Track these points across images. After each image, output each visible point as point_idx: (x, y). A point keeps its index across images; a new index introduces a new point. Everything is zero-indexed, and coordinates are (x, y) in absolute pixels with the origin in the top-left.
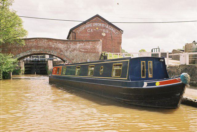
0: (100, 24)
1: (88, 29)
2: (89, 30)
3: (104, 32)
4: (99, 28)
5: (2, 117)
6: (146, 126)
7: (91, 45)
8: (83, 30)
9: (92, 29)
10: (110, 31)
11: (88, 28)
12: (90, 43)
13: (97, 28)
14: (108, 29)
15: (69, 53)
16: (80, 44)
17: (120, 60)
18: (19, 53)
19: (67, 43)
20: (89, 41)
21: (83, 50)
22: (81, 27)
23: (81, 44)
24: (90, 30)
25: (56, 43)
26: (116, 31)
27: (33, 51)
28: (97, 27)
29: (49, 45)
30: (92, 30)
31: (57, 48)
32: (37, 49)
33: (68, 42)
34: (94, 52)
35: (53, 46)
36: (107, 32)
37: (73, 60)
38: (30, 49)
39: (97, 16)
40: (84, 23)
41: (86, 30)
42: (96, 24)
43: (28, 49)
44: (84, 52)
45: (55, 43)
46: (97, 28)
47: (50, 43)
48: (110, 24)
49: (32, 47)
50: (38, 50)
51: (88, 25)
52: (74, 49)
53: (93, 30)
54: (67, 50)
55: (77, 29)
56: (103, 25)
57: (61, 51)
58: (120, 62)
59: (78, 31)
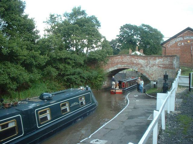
1: (179, 43)
2: (179, 44)
4: (191, 41)
5: (192, 88)
7: (169, 60)
8: (173, 44)
9: (183, 42)
11: (179, 42)
12: (169, 58)
13: (189, 42)
15: (149, 68)
16: (159, 60)
17: (11, 138)
21: (162, 66)
22: (171, 42)
24: (181, 44)
25: (138, 59)
27: (119, 66)
28: (189, 40)
30: (183, 43)
31: (139, 64)
32: (123, 65)
33: (148, 58)
35: (135, 62)
37: (152, 75)
38: (116, 65)
39: (189, 29)
40: (175, 37)
41: (176, 43)
43: (115, 65)
44: (163, 67)
45: (136, 59)
46: (189, 42)
47: (133, 59)
50: (123, 66)
51: (178, 39)
52: (154, 65)
54: (146, 66)
55: (168, 44)
57: (142, 66)
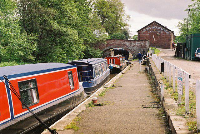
0: (157, 27)
3: (135, 41)
6: (35, 124)
10: (163, 31)
14: (161, 30)
16: (137, 43)
18: (104, 48)
19: (130, 42)
20: (143, 41)
23: (138, 42)
24: (150, 32)
25: (124, 42)
26: (168, 31)
29: (120, 43)
31: (125, 45)
34: (145, 47)
35: (123, 44)
36: (161, 32)
39: (154, 22)
42: (154, 27)
47: (121, 42)
48: (163, 27)
49: (111, 44)
51: (148, 28)
52: (135, 46)
53: (152, 32)
56: (158, 27)
57: (127, 46)
58: (9, 97)
59: (142, 32)
